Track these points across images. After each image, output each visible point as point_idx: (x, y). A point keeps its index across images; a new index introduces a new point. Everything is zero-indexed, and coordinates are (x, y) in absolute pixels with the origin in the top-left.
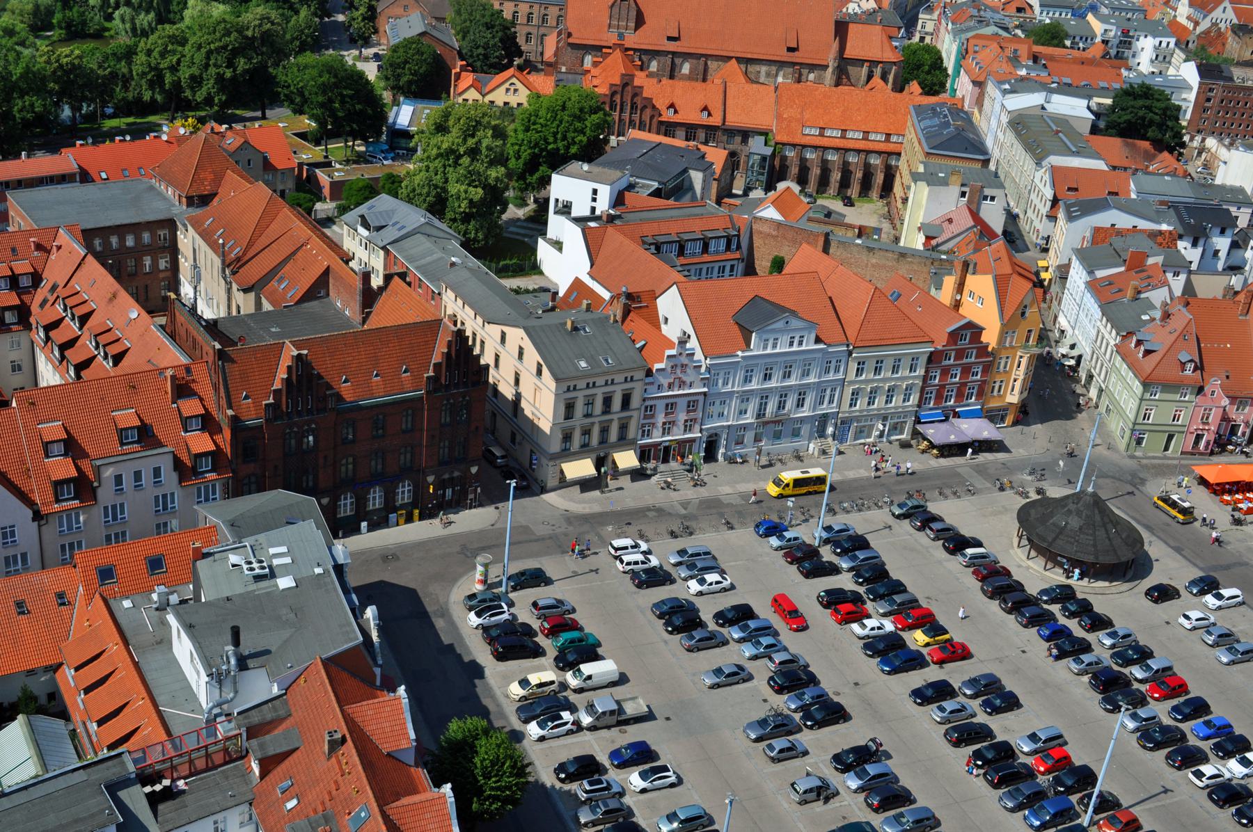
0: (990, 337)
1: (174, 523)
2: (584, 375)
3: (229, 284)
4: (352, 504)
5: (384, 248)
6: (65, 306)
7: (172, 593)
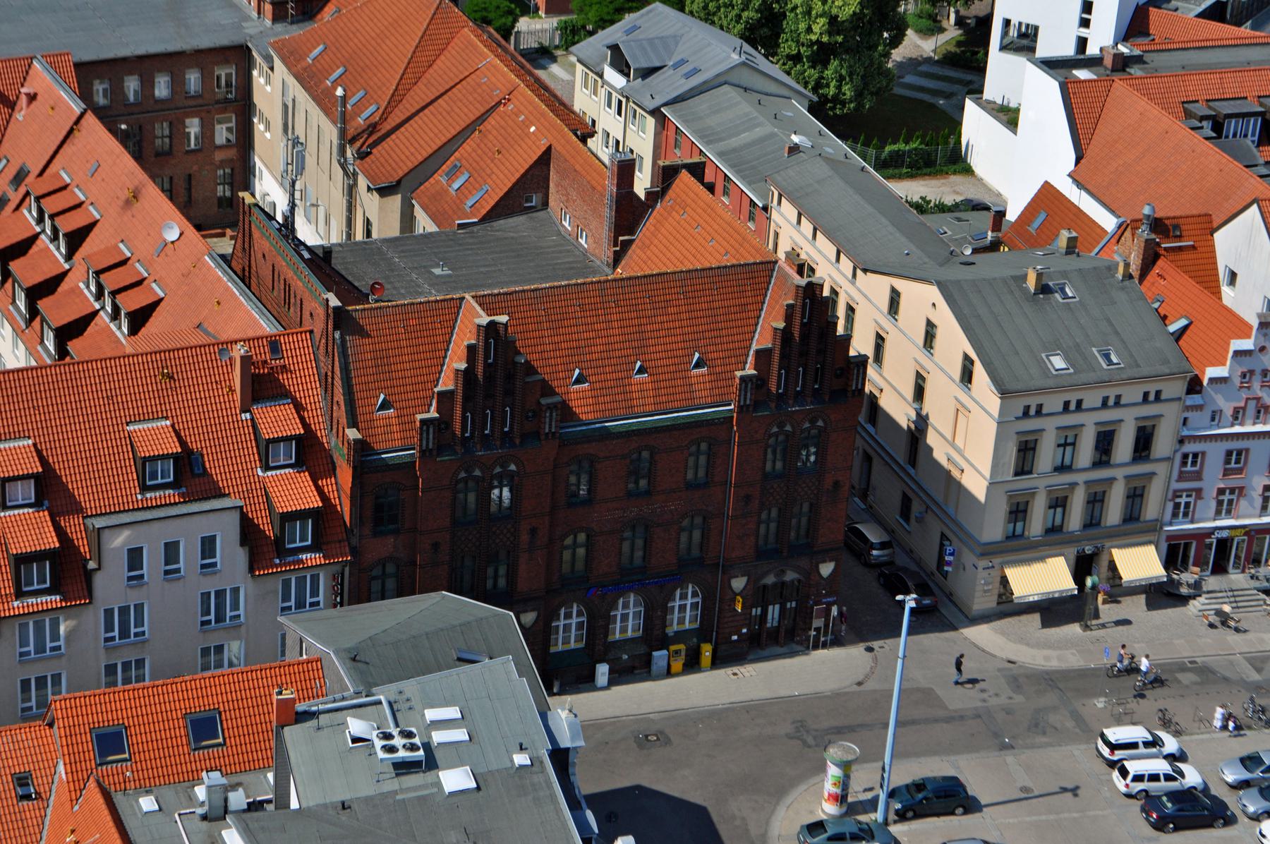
1: (234, 648)
2: (1059, 384)
3: (351, 177)
4: (580, 626)
5: (655, 112)
6: (41, 212)
7: (233, 787)
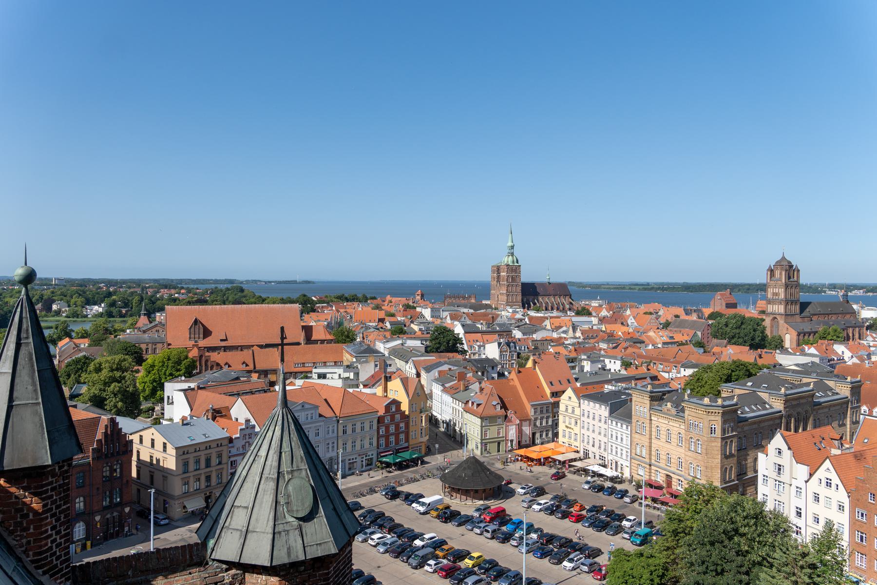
0: (405, 407)
